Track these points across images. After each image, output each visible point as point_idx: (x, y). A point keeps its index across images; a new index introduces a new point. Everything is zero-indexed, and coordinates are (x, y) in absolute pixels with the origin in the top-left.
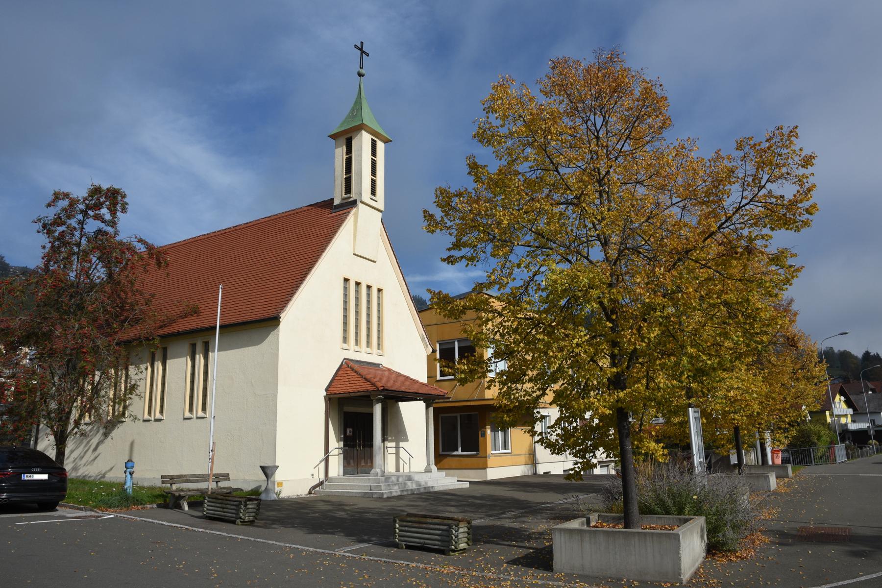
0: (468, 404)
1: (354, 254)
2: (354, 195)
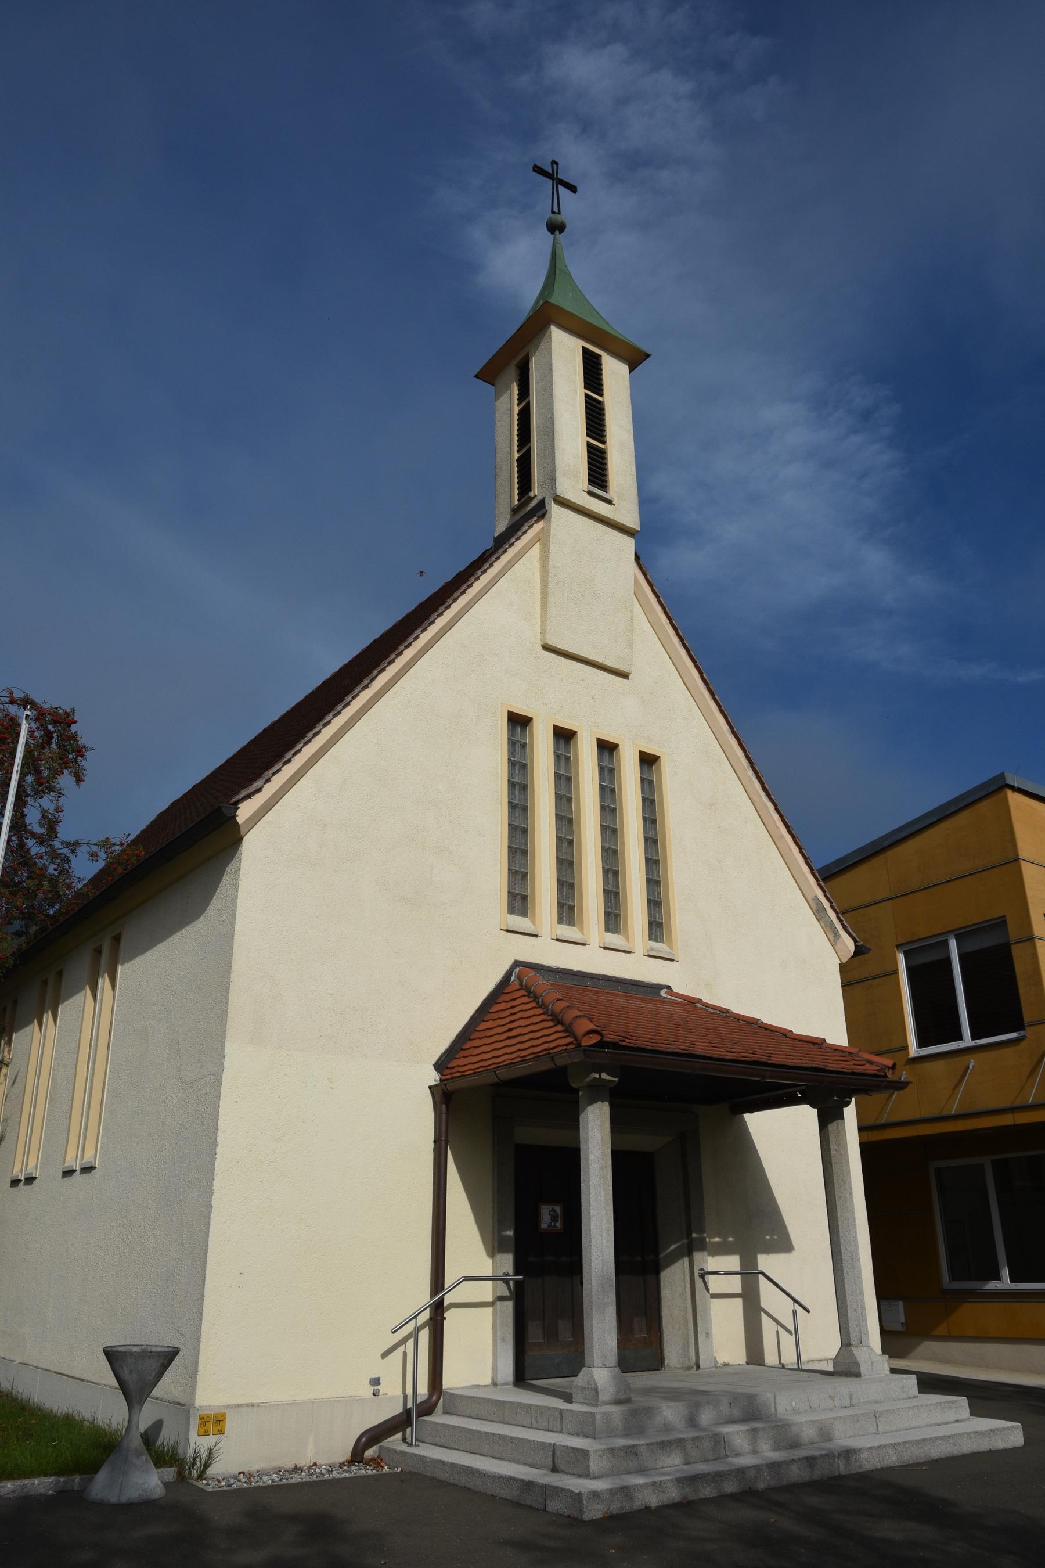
0: (1007, 1120)
1: (547, 648)
2: (537, 491)
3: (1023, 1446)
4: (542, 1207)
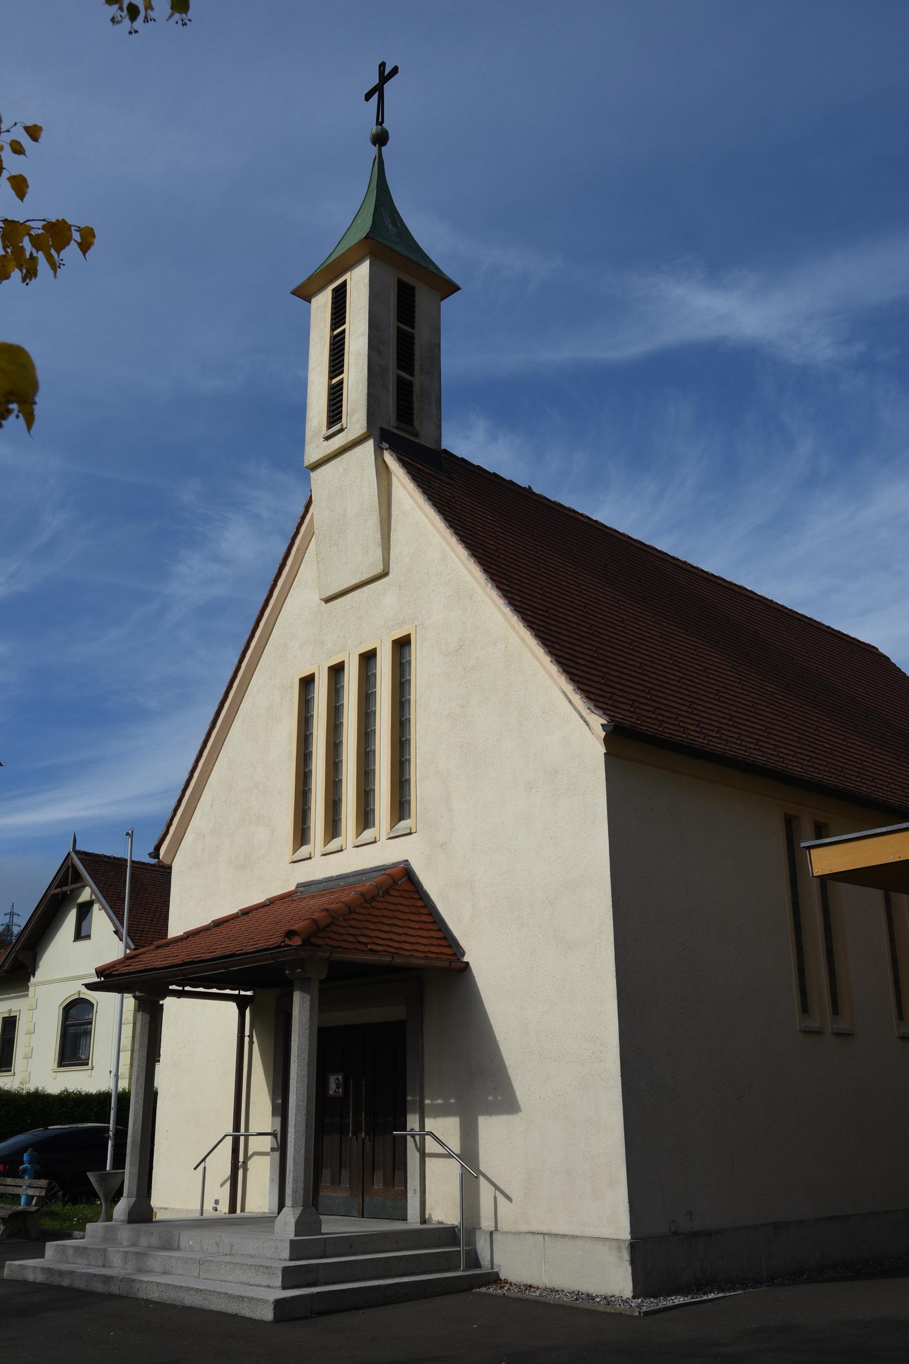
3: (271, 1322)
4: (331, 1077)
